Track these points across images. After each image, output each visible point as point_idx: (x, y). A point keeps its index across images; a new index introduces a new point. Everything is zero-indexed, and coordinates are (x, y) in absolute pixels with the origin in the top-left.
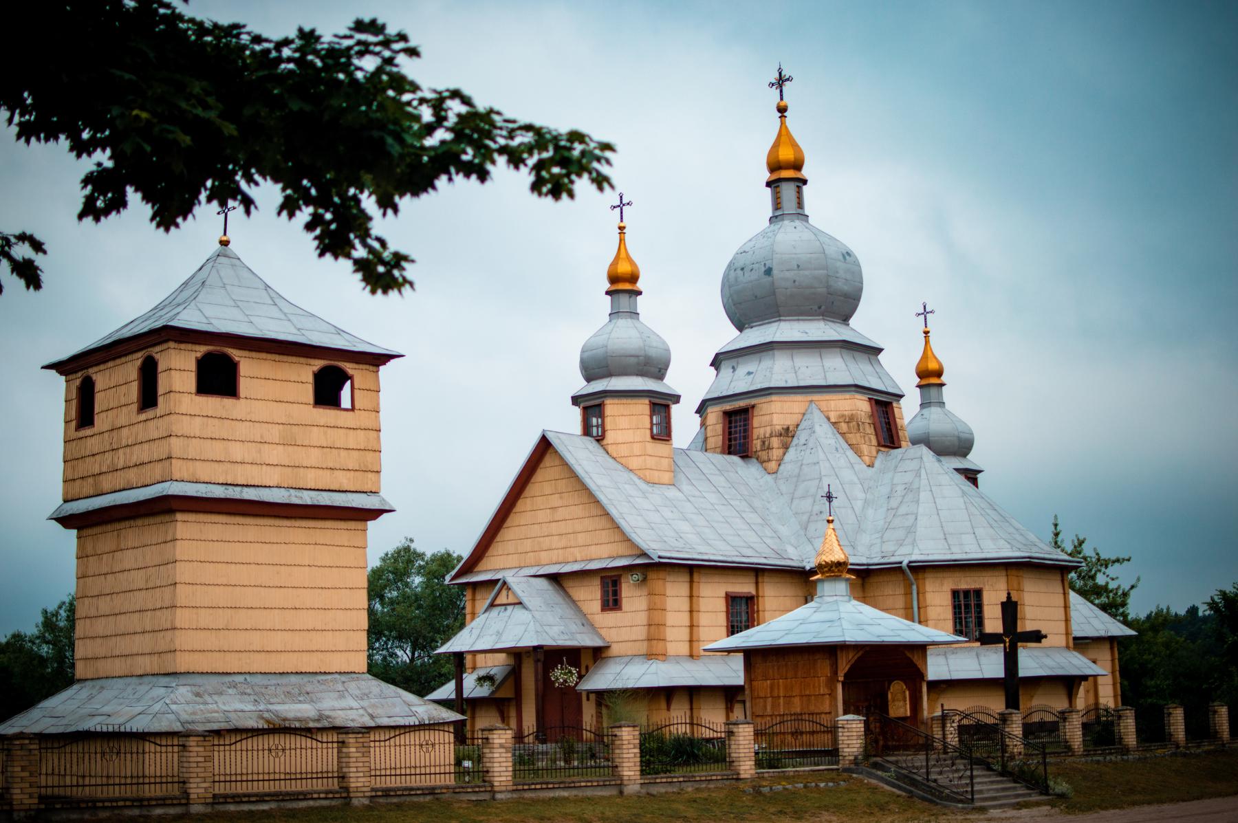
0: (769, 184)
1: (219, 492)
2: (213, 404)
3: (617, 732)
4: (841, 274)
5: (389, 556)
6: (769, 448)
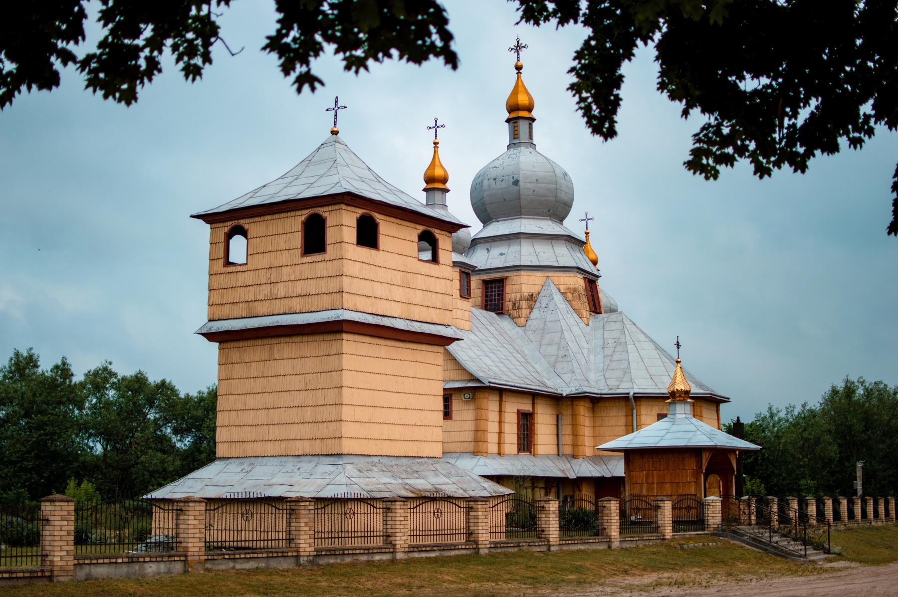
0: (508, 121)
1: (371, 320)
2: (365, 252)
3: (661, 504)
4: (564, 188)
5: (91, 373)
6: (519, 308)
